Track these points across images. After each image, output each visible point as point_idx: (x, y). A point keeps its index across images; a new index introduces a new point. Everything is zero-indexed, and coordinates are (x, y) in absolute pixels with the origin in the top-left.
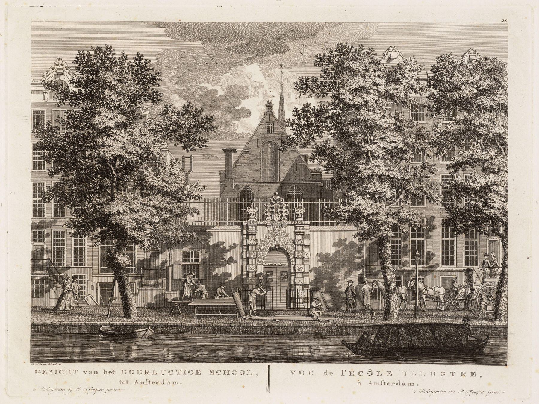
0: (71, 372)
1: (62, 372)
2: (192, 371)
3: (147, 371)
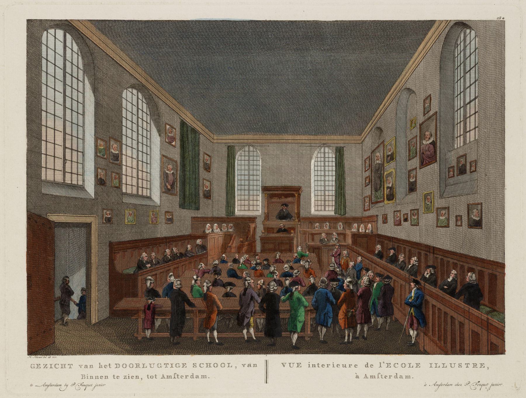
0: (66, 366)
1: (57, 366)
2: (161, 364)
3: (475, 365)
